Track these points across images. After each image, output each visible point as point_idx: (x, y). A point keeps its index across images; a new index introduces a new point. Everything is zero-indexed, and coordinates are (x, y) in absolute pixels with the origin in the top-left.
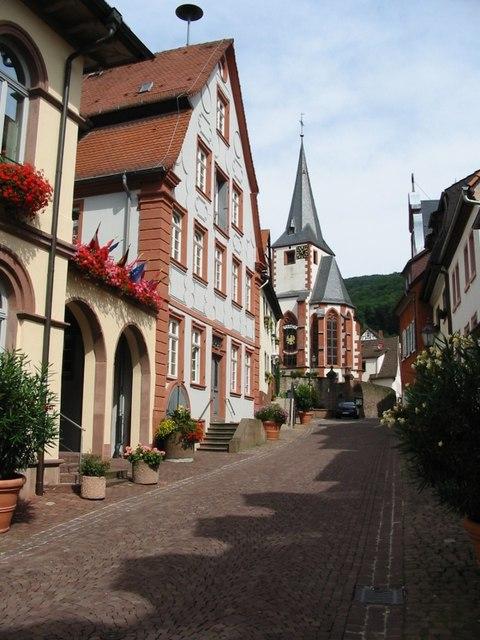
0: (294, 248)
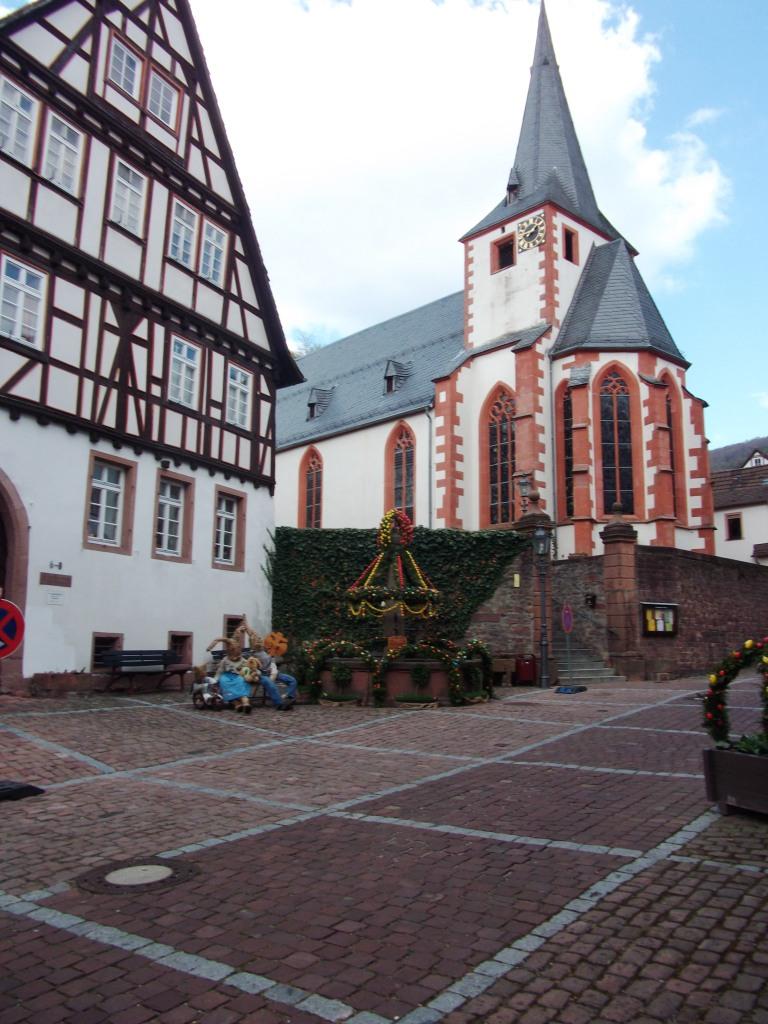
0: (511, 228)
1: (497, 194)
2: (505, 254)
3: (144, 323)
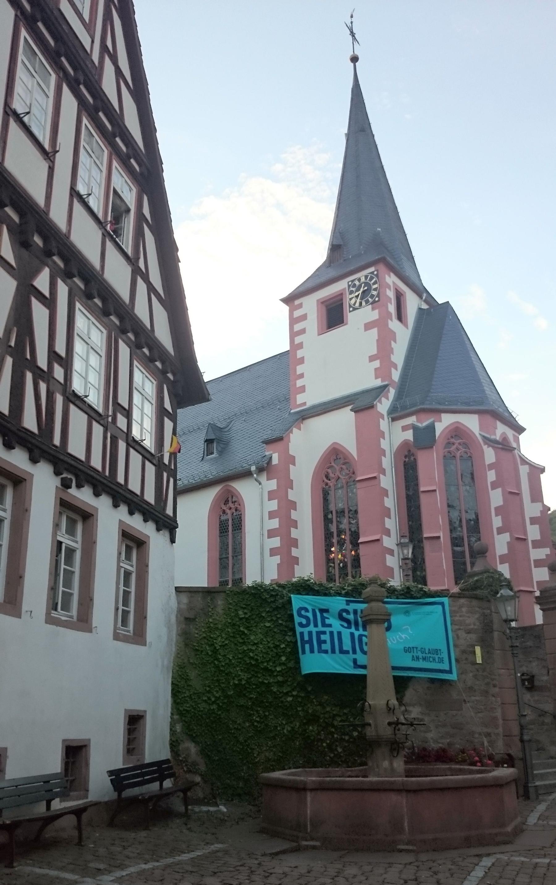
1: (316, 254)
2: (334, 315)
3: (45, 274)
